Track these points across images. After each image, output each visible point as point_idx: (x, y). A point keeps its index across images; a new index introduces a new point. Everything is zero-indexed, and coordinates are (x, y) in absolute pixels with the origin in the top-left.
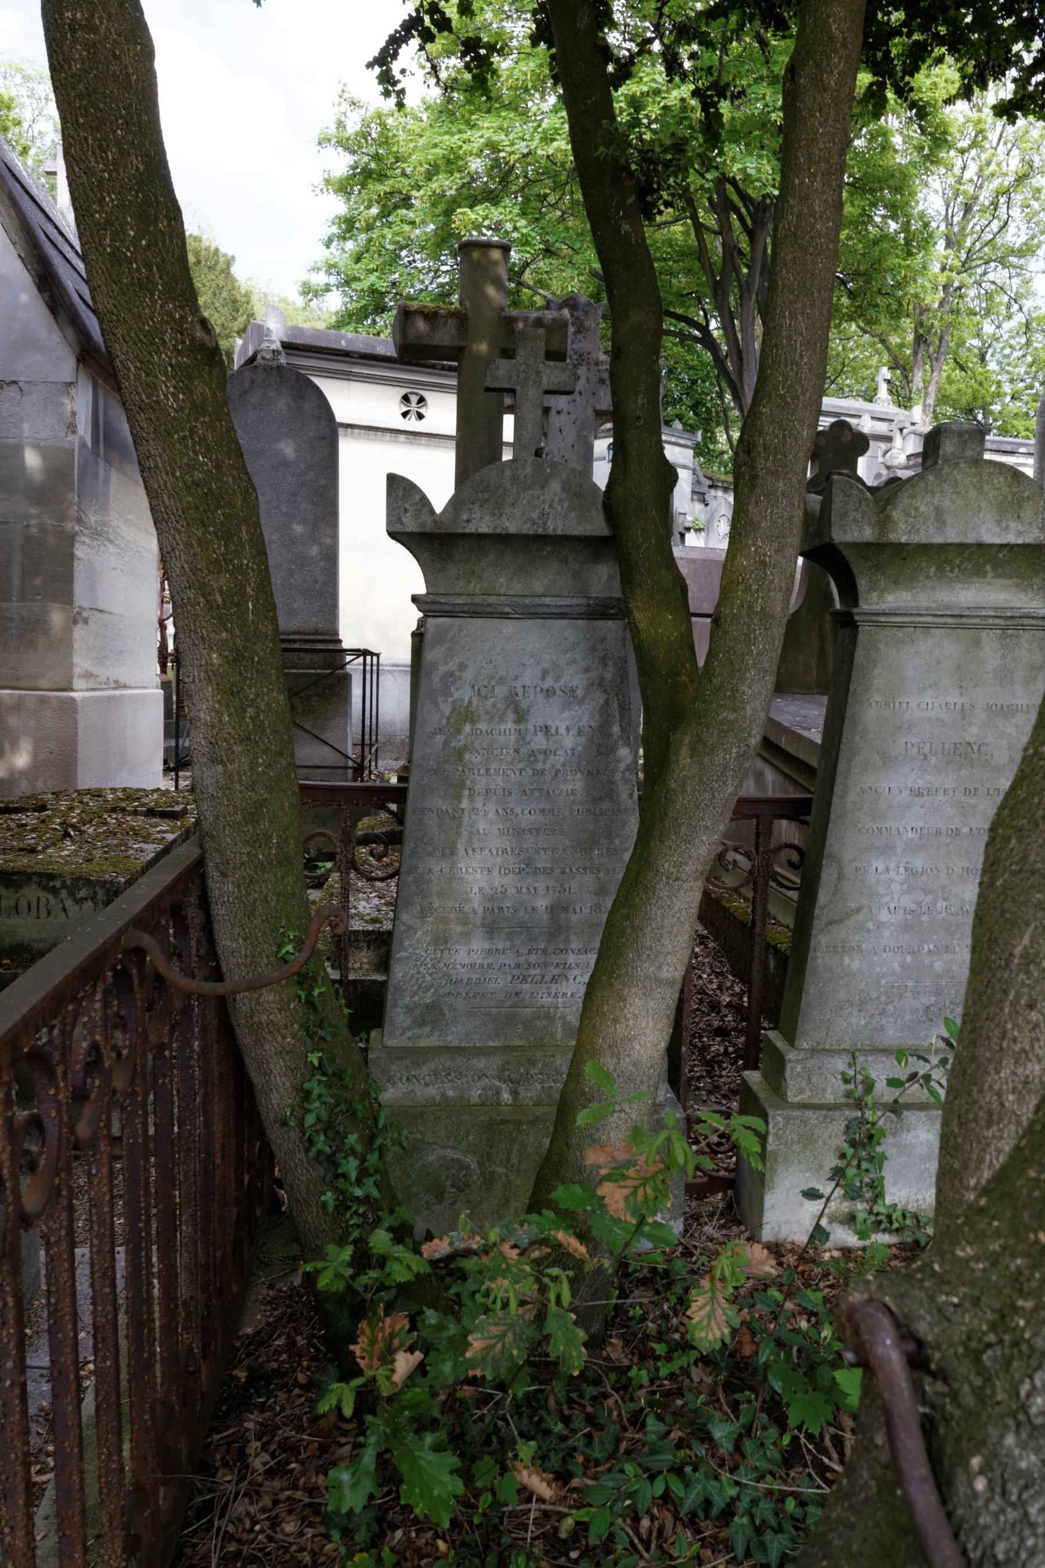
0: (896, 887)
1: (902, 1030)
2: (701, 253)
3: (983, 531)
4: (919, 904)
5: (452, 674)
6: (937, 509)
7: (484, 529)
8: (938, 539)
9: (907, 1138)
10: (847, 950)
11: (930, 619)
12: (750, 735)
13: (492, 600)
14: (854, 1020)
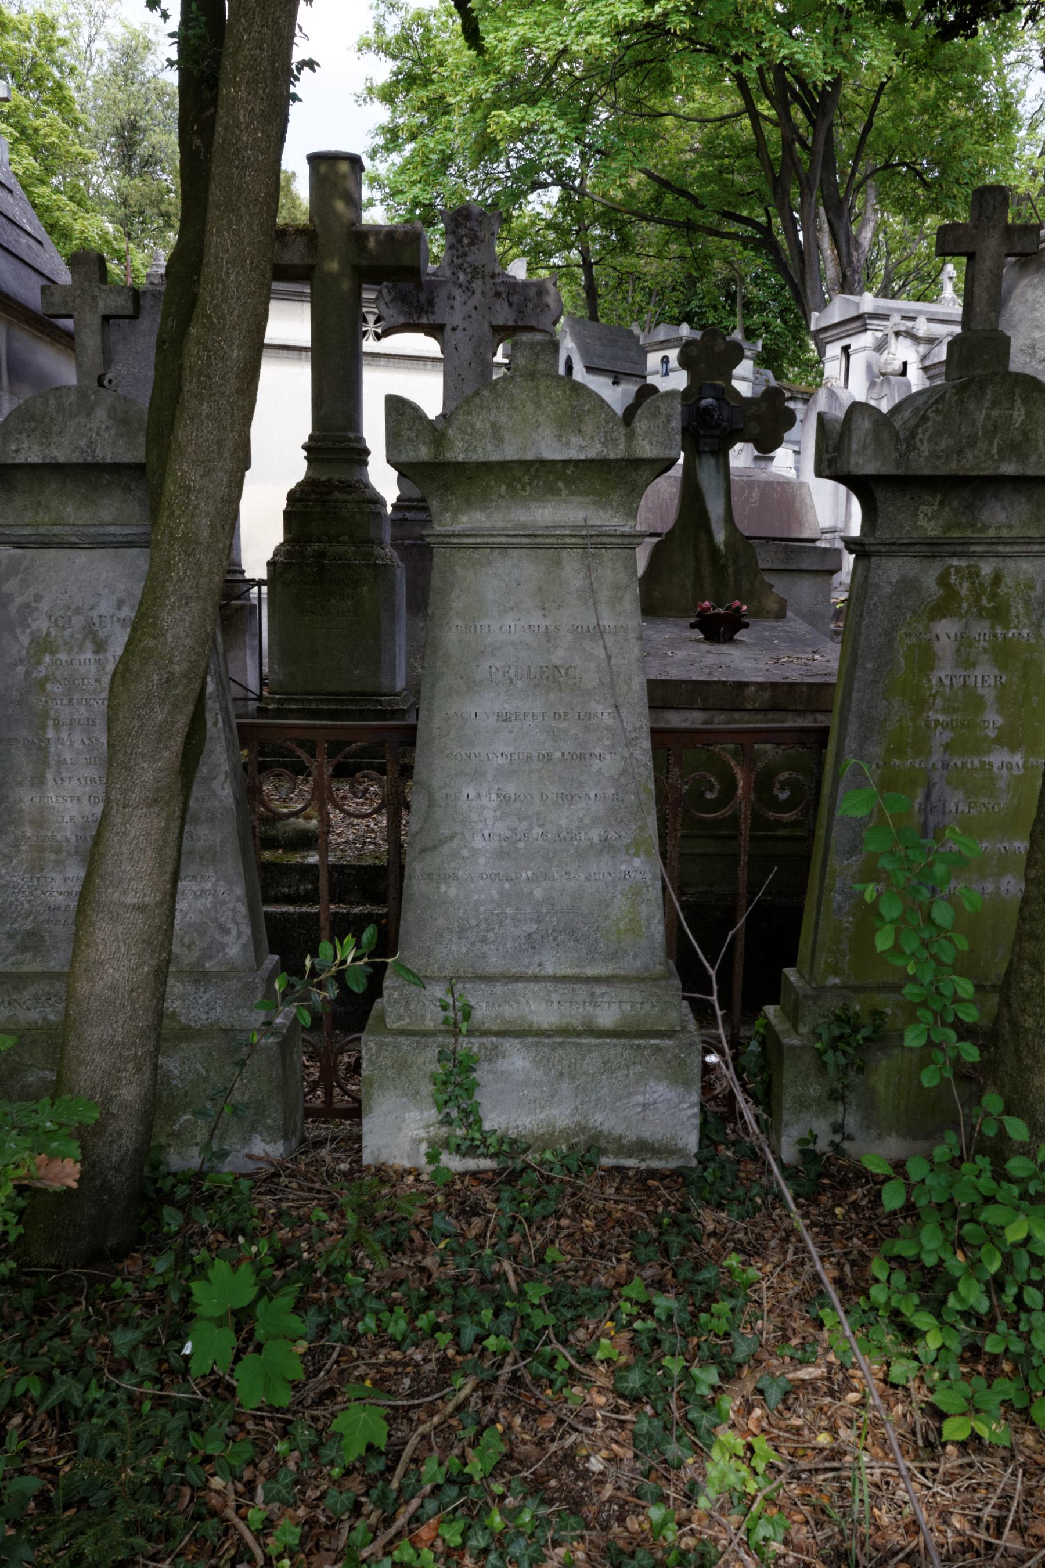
0: (489, 814)
1: (504, 958)
2: (760, 144)
3: (543, 447)
4: (514, 830)
5: (28, 605)
6: (494, 425)
7: (33, 459)
8: (496, 457)
9: (502, 1065)
11: (504, 540)
12: (171, 662)
13: (56, 530)
14: (454, 948)
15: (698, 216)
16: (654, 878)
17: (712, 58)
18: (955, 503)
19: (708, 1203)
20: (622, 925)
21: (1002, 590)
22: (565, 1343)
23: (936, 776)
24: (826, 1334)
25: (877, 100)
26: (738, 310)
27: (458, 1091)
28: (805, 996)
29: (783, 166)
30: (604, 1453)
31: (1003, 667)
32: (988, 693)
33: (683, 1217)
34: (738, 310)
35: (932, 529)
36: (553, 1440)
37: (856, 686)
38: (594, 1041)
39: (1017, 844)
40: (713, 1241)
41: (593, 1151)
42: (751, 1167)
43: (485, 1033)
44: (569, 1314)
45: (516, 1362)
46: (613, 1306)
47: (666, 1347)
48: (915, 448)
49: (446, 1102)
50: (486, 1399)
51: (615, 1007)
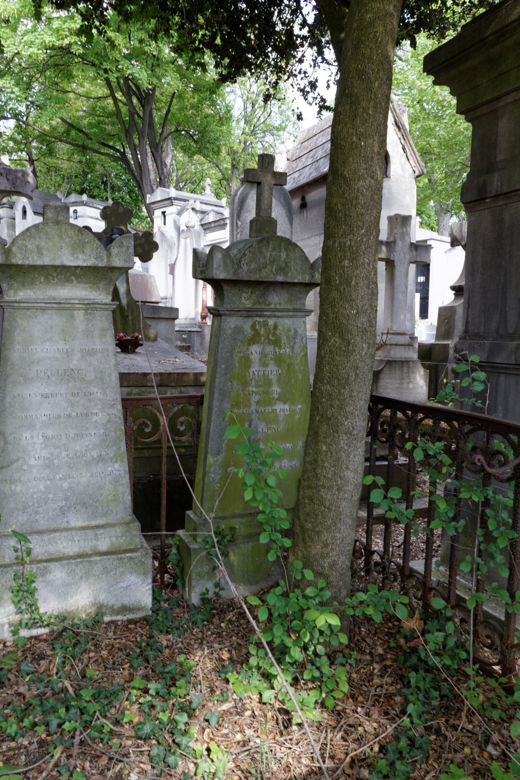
0: (38, 446)
1: (48, 521)
2: (118, 113)
3: (64, 259)
4: (52, 454)
6: (38, 247)
8: (39, 263)
9: (50, 577)
10: (13, 481)
14: (20, 518)
15: (88, 142)
16: (125, 473)
17: (94, 68)
18: (257, 293)
19: (161, 632)
20: (109, 498)
21: (278, 332)
22: (105, 717)
23: (253, 416)
24: (231, 686)
25: (172, 100)
26: (108, 189)
27: (25, 594)
28: (200, 524)
29: (130, 124)
30: (137, 770)
31: (279, 366)
32: (274, 378)
33: (151, 641)
34: (108, 189)
35: (248, 304)
36: (109, 770)
37: (217, 376)
38: (98, 558)
39: (288, 445)
40: (167, 650)
41: (100, 615)
42: (178, 610)
43: (39, 562)
44: (106, 702)
45: (81, 733)
46: (127, 693)
47: (158, 708)
48: (241, 267)
49: (19, 601)
50: (69, 757)
51: (108, 540)
